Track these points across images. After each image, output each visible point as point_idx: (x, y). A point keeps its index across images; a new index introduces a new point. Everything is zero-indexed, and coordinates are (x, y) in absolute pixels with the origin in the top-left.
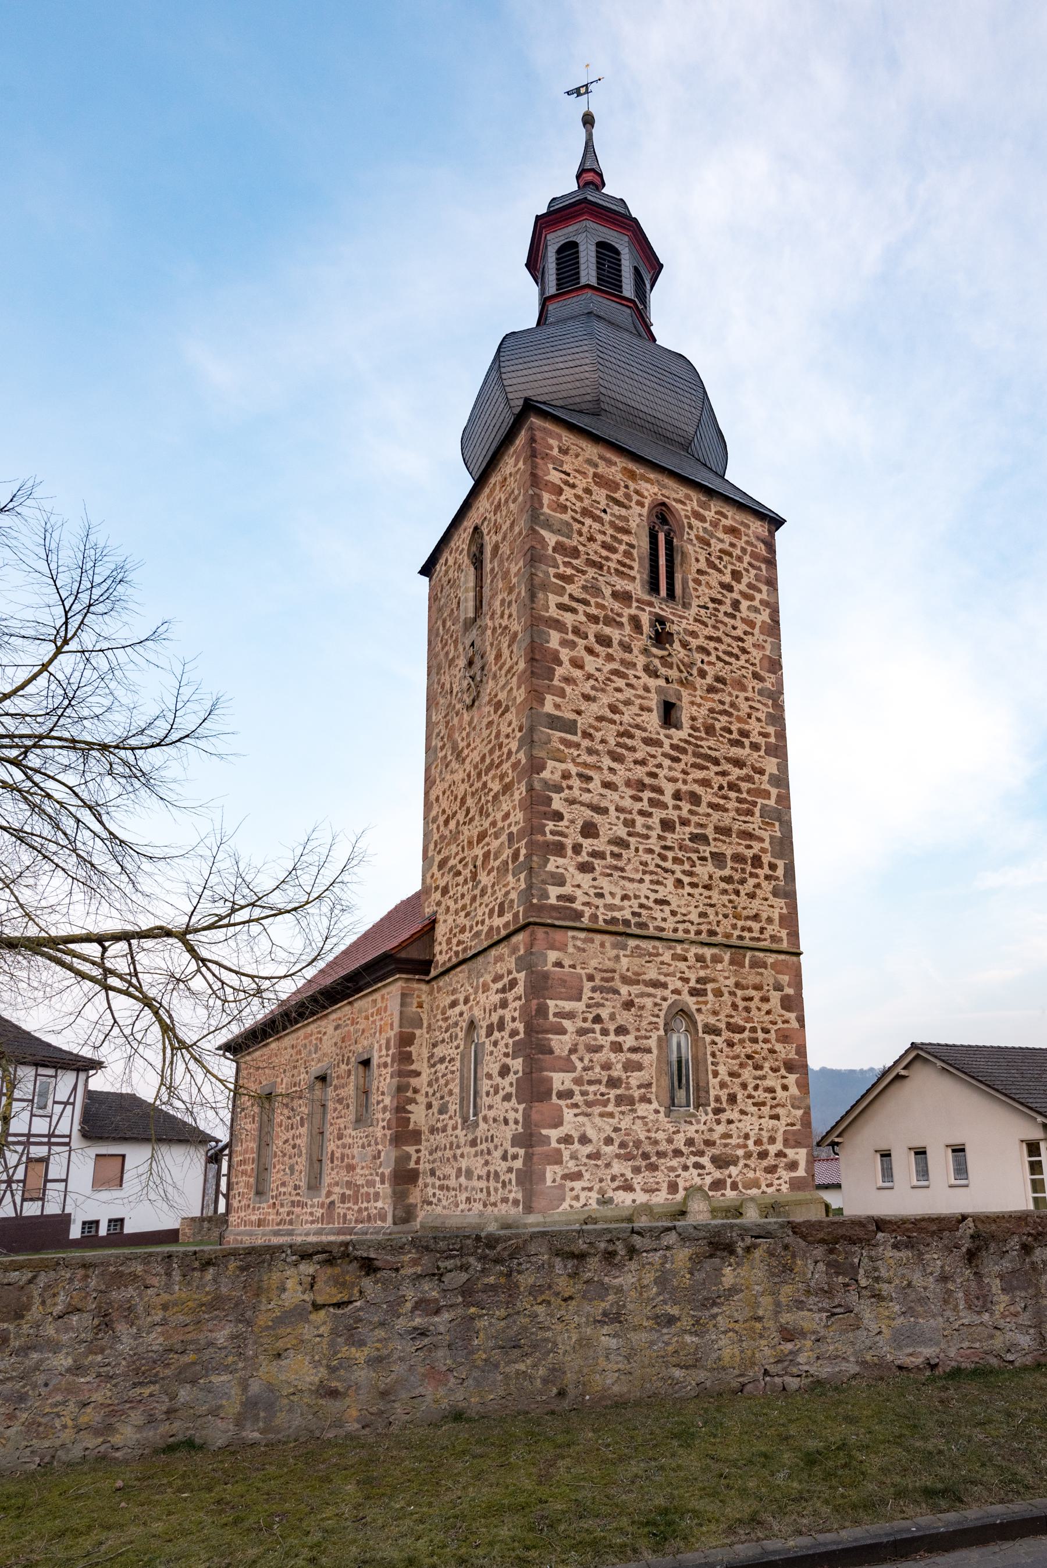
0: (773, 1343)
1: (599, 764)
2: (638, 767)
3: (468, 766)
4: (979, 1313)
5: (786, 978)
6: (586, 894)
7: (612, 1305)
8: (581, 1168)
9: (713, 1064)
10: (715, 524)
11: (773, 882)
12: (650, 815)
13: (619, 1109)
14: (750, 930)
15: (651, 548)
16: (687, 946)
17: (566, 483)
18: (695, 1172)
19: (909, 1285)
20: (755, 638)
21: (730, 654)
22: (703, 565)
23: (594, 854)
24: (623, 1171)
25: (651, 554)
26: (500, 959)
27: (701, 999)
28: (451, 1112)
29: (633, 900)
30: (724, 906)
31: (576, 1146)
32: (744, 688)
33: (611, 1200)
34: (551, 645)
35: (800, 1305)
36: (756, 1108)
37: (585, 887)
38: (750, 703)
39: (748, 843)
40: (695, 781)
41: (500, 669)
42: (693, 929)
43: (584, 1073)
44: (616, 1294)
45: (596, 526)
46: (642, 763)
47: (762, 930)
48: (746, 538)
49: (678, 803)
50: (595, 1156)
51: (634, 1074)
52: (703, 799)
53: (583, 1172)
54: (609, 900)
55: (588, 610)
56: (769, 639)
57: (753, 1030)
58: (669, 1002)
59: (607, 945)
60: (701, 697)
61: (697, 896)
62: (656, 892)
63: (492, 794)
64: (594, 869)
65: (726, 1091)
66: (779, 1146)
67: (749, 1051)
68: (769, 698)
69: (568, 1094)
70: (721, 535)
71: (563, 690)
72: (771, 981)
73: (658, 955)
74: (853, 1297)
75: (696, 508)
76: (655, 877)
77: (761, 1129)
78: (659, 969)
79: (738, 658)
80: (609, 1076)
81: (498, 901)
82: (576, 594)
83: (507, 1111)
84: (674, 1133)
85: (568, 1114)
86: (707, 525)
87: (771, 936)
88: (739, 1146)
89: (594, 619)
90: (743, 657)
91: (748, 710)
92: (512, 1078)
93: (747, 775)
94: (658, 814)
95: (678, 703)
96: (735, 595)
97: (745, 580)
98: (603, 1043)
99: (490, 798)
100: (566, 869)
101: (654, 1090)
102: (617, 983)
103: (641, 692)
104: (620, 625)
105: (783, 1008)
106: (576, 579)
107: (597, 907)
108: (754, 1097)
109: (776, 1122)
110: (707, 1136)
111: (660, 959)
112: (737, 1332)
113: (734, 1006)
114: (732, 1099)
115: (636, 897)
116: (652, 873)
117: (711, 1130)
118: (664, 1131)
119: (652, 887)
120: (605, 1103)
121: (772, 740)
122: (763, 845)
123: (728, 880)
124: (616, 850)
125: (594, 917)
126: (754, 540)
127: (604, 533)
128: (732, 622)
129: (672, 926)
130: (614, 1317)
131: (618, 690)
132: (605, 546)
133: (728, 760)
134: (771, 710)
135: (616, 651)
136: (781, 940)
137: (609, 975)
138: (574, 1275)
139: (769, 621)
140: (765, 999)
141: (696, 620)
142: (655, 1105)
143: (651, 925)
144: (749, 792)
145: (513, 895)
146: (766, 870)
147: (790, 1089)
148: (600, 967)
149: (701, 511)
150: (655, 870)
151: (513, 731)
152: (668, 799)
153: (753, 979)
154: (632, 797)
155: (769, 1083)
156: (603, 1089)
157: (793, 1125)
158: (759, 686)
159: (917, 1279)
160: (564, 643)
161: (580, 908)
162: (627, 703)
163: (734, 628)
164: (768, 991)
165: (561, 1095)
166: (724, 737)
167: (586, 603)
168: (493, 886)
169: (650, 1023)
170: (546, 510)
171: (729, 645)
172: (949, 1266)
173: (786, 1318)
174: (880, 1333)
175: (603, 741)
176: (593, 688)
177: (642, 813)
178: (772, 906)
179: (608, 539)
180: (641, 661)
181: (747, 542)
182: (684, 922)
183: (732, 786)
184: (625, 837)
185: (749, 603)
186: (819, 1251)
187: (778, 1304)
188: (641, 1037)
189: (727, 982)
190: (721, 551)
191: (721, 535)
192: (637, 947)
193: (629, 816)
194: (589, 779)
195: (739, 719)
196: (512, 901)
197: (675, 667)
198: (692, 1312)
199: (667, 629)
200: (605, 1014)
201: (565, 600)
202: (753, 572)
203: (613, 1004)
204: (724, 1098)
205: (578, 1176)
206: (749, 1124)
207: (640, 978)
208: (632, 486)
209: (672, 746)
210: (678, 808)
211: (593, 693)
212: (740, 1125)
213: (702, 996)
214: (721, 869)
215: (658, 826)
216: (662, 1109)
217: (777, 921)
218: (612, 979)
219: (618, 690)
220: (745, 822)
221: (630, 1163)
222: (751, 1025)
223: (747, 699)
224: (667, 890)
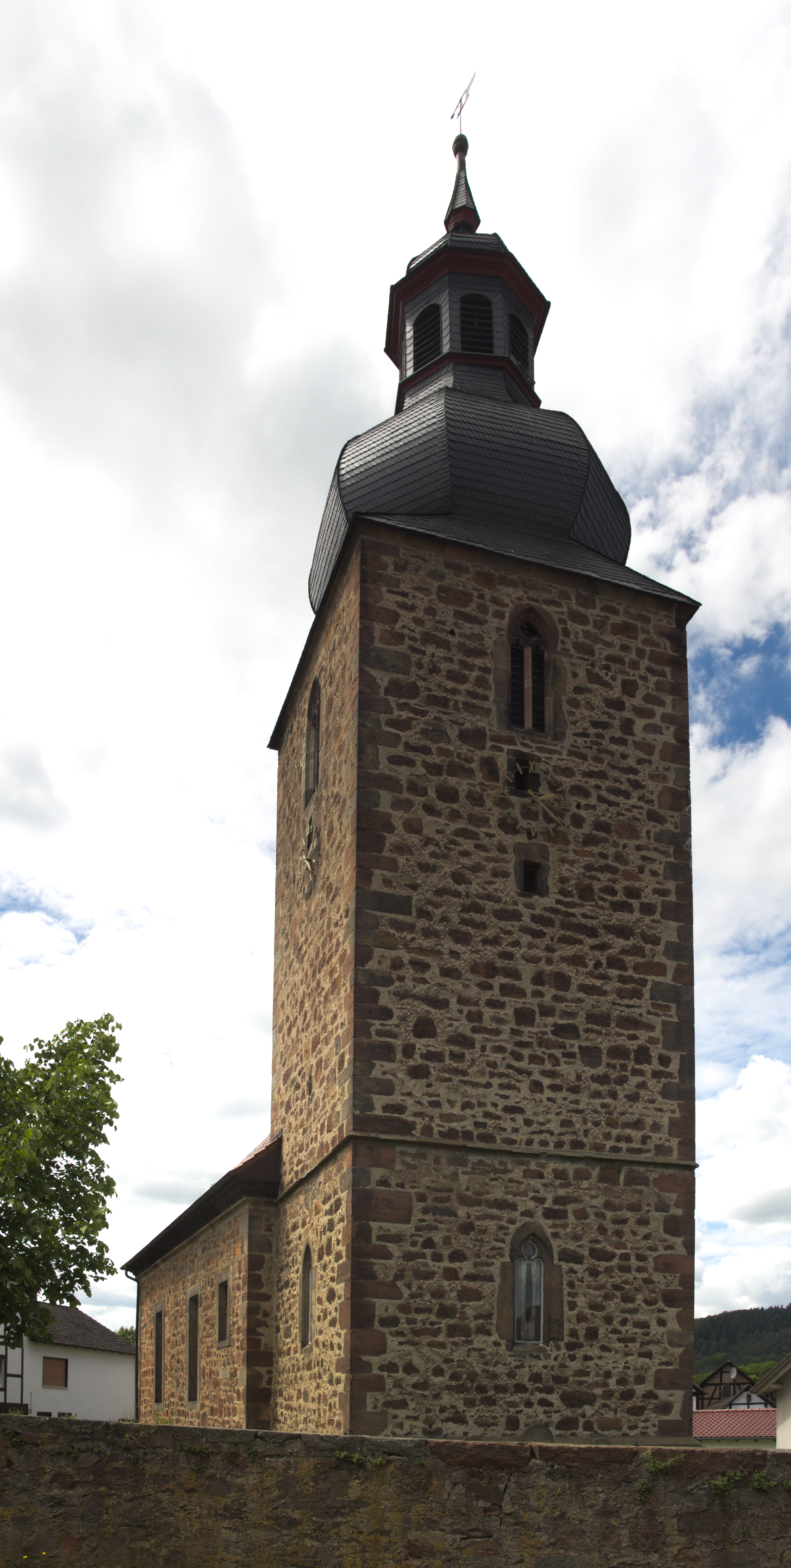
0: (399, 1557)
1: (438, 948)
2: (489, 948)
3: (306, 965)
4: (646, 1553)
5: (674, 1196)
6: (419, 1103)
7: (233, 1501)
8: (406, 1396)
9: (569, 1294)
10: (600, 625)
11: (664, 1080)
12: (502, 1005)
13: (452, 1340)
14: (629, 1139)
15: (513, 669)
16: (543, 1161)
17: (403, 606)
18: (540, 1409)
19: (562, 1515)
20: (654, 767)
21: (617, 792)
22: (582, 679)
23: (430, 1056)
24: (454, 1403)
25: (513, 677)
26: (328, 1178)
27: (557, 1222)
28: (293, 1337)
29: (477, 1109)
30: (595, 1111)
31: (401, 1374)
32: (635, 835)
33: (438, 1432)
34: (381, 809)
35: (431, 1524)
36: (622, 1345)
37: (418, 1094)
38: (643, 853)
39: (632, 1032)
40: (563, 959)
41: (332, 846)
42: (552, 1140)
43: (411, 1301)
44: (237, 1492)
45: (441, 653)
46: (494, 941)
47: (644, 1140)
48: (645, 636)
49: (540, 988)
50: (423, 1385)
51: (472, 1303)
52: (573, 980)
53: (408, 1401)
54: (446, 1109)
55: (429, 759)
56: (673, 766)
57: (625, 1257)
58: (518, 1225)
59: (443, 1160)
60: (575, 852)
61: (560, 1101)
62: (507, 1097)
63: (324, 994)
64: (429, 1073)
65: (585, 1325)
66: (648, 1386)
67: (618, 1280)
68: (670, 843)
69: (392, 1322)
70: (608, 638)
71: (395, 862)
72: (653, 1201)
73: (506, 1171)
74: (494, 1523)
75: (575, 607)
76: (505, 1081)
77: (626, 1368)
78: (506, 1187)
79: (627, 796)
80: (441, 1304)
81: (328, 1114)
82: (413, 742)
83: (333, 1335)
84: (516, 1367)
85: (392, 1342)
86: (589, 628)
87: (656, 1147)
88: (597, 1385)
89: (434, 769)
90: (635, 794)
91: (640, 862)
92: (337, 1302)
93: (635, 946)
94: (512, 1003)
95: (544, 862)
96: (627, 714)
97: (641, 692)
98: (435, 1269)
99: (322, 999)
100: (395, 1075)
101: (494, 1321)
102: (454, 1203)
103: (494, 854)
104: (469, 773)
105: (667, 1231)
106: (414, 722)
107: (432, 1118)
108: (620, 1332)
109: (647, 1360)
110: (557, 1372)
111: (510, 1175)
112: (360, 1543)
113: (602, 1230)
114: (592, 1334)
115: (481, 1105)
116: (501, 1075)
117: (563, 1366)
118: (505, 1364)
119: (501, 1092)
120: (438, 1331)
121: (673, 898)
122: (652, 1034)
123: (602, 1079)
124: (456, 1049)
125: (427, 1130)
126: (655, 637)
127: (451, 660)
128: (622, 749)
129: (525, 1138)
130: (236, 1513)
131: (465, 854)
132: (452, 676)
133: (609, 929)
134: (672, 860)
135: (463, 806)
136: (669, 1150)
137: (445, 1194)
138: (199, 1471)
139: (674, 742)
140: (643, 1222)
141: (571, 753)
142: (495, 1337)
143: (498, 1138)
144: (636, 968)
145: (339, 1108)
146: (655, 1065)
147: (669, 1325)
148: (434, 1185)
149: (582, 610)
150: (506, 1071)
151: (341, 917)
152: (526, 984)
153: (628, 1198)
154: (479, 985)
155: (641, 1317)
156: (433, 1318)
157: (668, 1364)
158: (655, 828)
159: (573, 1511)
160: (397, 804)
161: (411, 1119)
162: (477, 868)
163: (624, 757)
164: (648, 1211)
165: (384, 1322)
166: (605, 900)
167: (426, 751)
168: (324, 1099)
169: (493, 1248)
170: (378, 644)
171: (616, 780)
172: (614, 1500)
173: (413, 1535)
174: (521, 1561)
175: (444, 919)
176: (433, 855)
177: (491, 1003)
178: (660, 1110)
179: (456, 667)
180: (495, 814)
181: (646, 642)
182: (541, 1132)
183: (613, 962)
184: (469, 1033)
185: (645, 721)
186: (458, 1474)
187: (407, 1521)
188: (482, 1264)
189: (594, 1202)
190: (609, 658)
191: (608, 638)
192: (480, 1163)
193: (474, 1009)
194: (425, 967)
195: (627, 876)
196: (338, 1113)
197: (541, 817)
198: (314, 1518)
199: (531, 769)
200: (437, 1237)
201: (400, 750)
202: (654, 679)
203: (448, 1227)
204: (582, 1333)
205: (403, 1404)
206: (613, 1362)
207: (483, 1198)
208: (488, 593)
209: (534, 918)
210: (538, 994)
211: (432, 861)
212: (600, 1362)
213: (560, 1218)
214: (592, 1067)
215: (512, 1019)
216: (503, 1342)
217: (666, 1129)
218: (448, 1199)
219: (465, 854)
220: (628, 1006)
221: (462, 1396)
222: (623, 1251)
223: (639, 848)
224: (521, 1095)
